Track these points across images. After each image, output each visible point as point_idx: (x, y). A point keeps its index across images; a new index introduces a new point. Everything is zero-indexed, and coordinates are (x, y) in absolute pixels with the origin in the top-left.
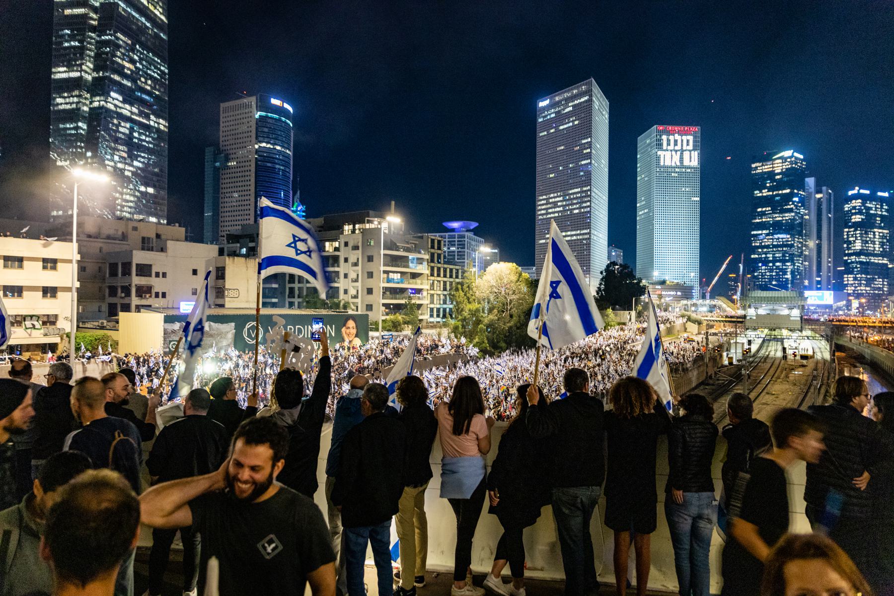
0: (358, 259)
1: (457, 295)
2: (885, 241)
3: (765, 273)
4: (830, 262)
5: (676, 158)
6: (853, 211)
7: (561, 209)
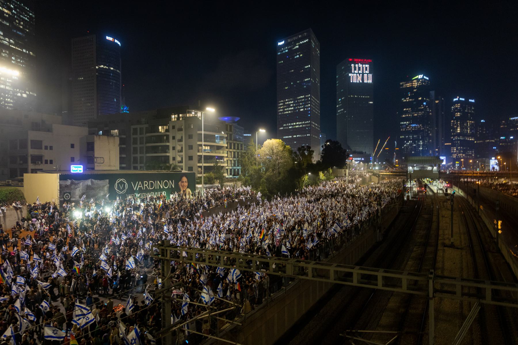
0: (182, 137)
1: (244, 160)
2: (473, 128)
3: (408, 146)
4: (443, 140)
5: (360, 78)
6: (456, 110)
7: (293, 108)
